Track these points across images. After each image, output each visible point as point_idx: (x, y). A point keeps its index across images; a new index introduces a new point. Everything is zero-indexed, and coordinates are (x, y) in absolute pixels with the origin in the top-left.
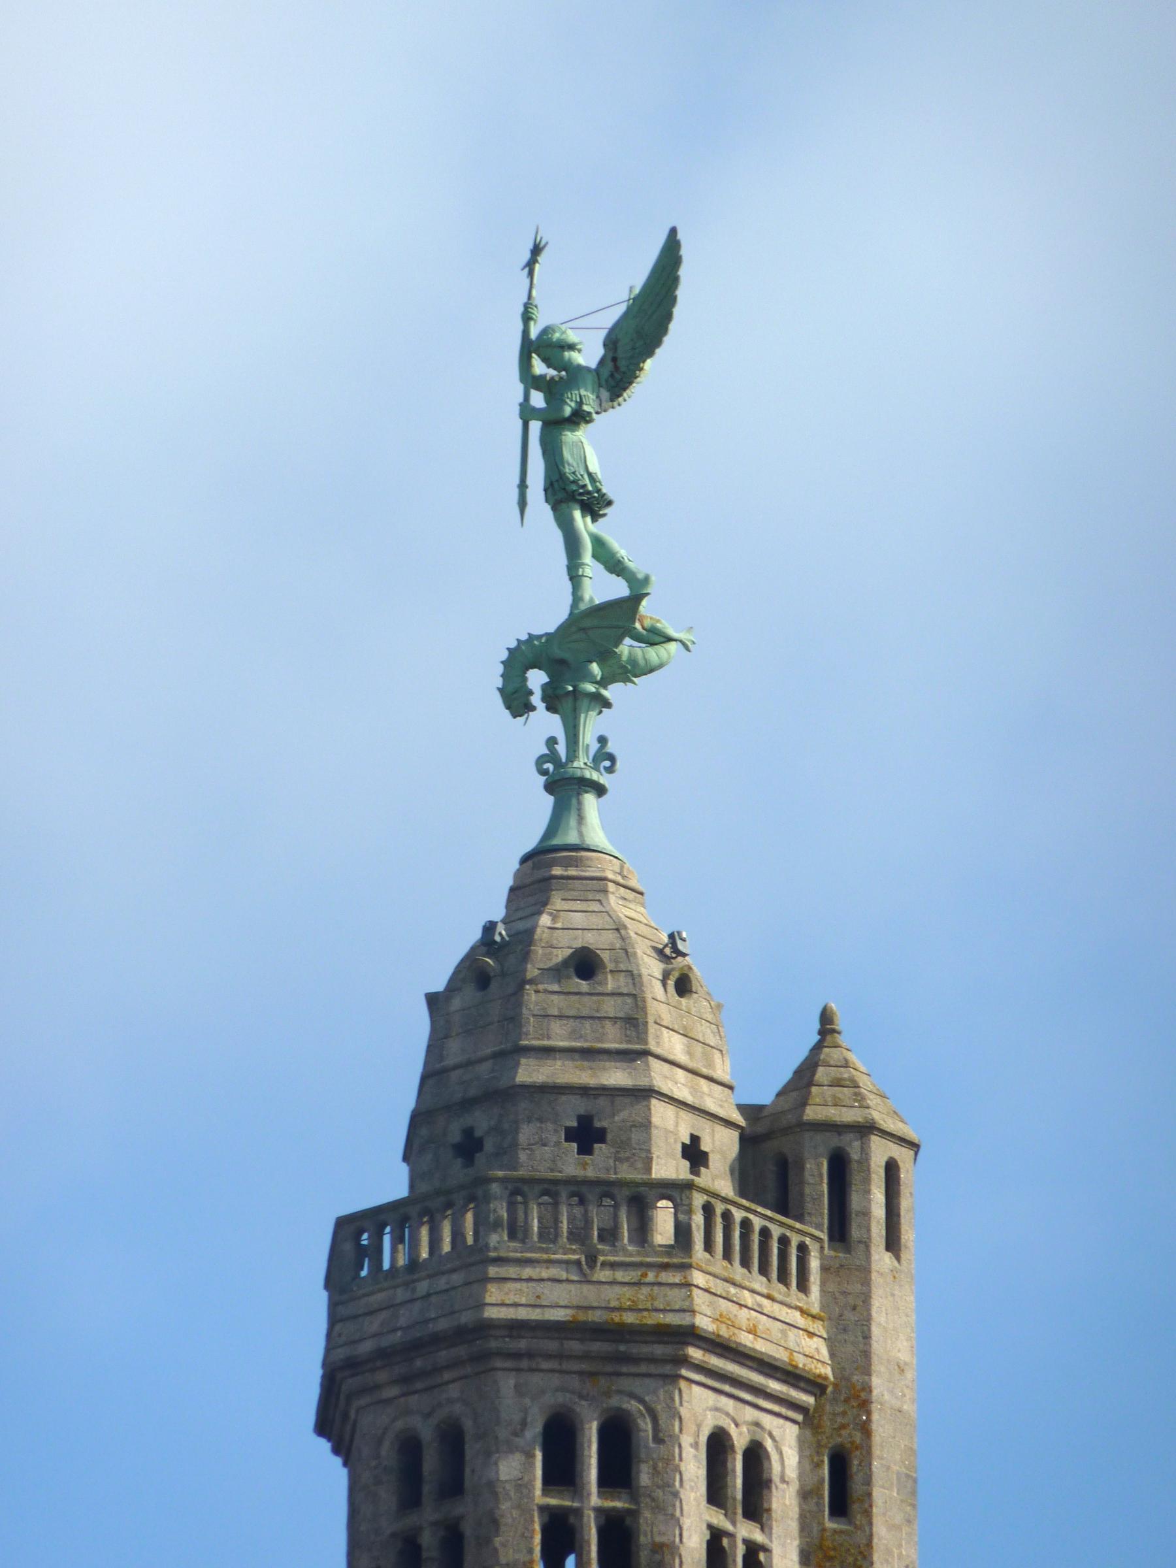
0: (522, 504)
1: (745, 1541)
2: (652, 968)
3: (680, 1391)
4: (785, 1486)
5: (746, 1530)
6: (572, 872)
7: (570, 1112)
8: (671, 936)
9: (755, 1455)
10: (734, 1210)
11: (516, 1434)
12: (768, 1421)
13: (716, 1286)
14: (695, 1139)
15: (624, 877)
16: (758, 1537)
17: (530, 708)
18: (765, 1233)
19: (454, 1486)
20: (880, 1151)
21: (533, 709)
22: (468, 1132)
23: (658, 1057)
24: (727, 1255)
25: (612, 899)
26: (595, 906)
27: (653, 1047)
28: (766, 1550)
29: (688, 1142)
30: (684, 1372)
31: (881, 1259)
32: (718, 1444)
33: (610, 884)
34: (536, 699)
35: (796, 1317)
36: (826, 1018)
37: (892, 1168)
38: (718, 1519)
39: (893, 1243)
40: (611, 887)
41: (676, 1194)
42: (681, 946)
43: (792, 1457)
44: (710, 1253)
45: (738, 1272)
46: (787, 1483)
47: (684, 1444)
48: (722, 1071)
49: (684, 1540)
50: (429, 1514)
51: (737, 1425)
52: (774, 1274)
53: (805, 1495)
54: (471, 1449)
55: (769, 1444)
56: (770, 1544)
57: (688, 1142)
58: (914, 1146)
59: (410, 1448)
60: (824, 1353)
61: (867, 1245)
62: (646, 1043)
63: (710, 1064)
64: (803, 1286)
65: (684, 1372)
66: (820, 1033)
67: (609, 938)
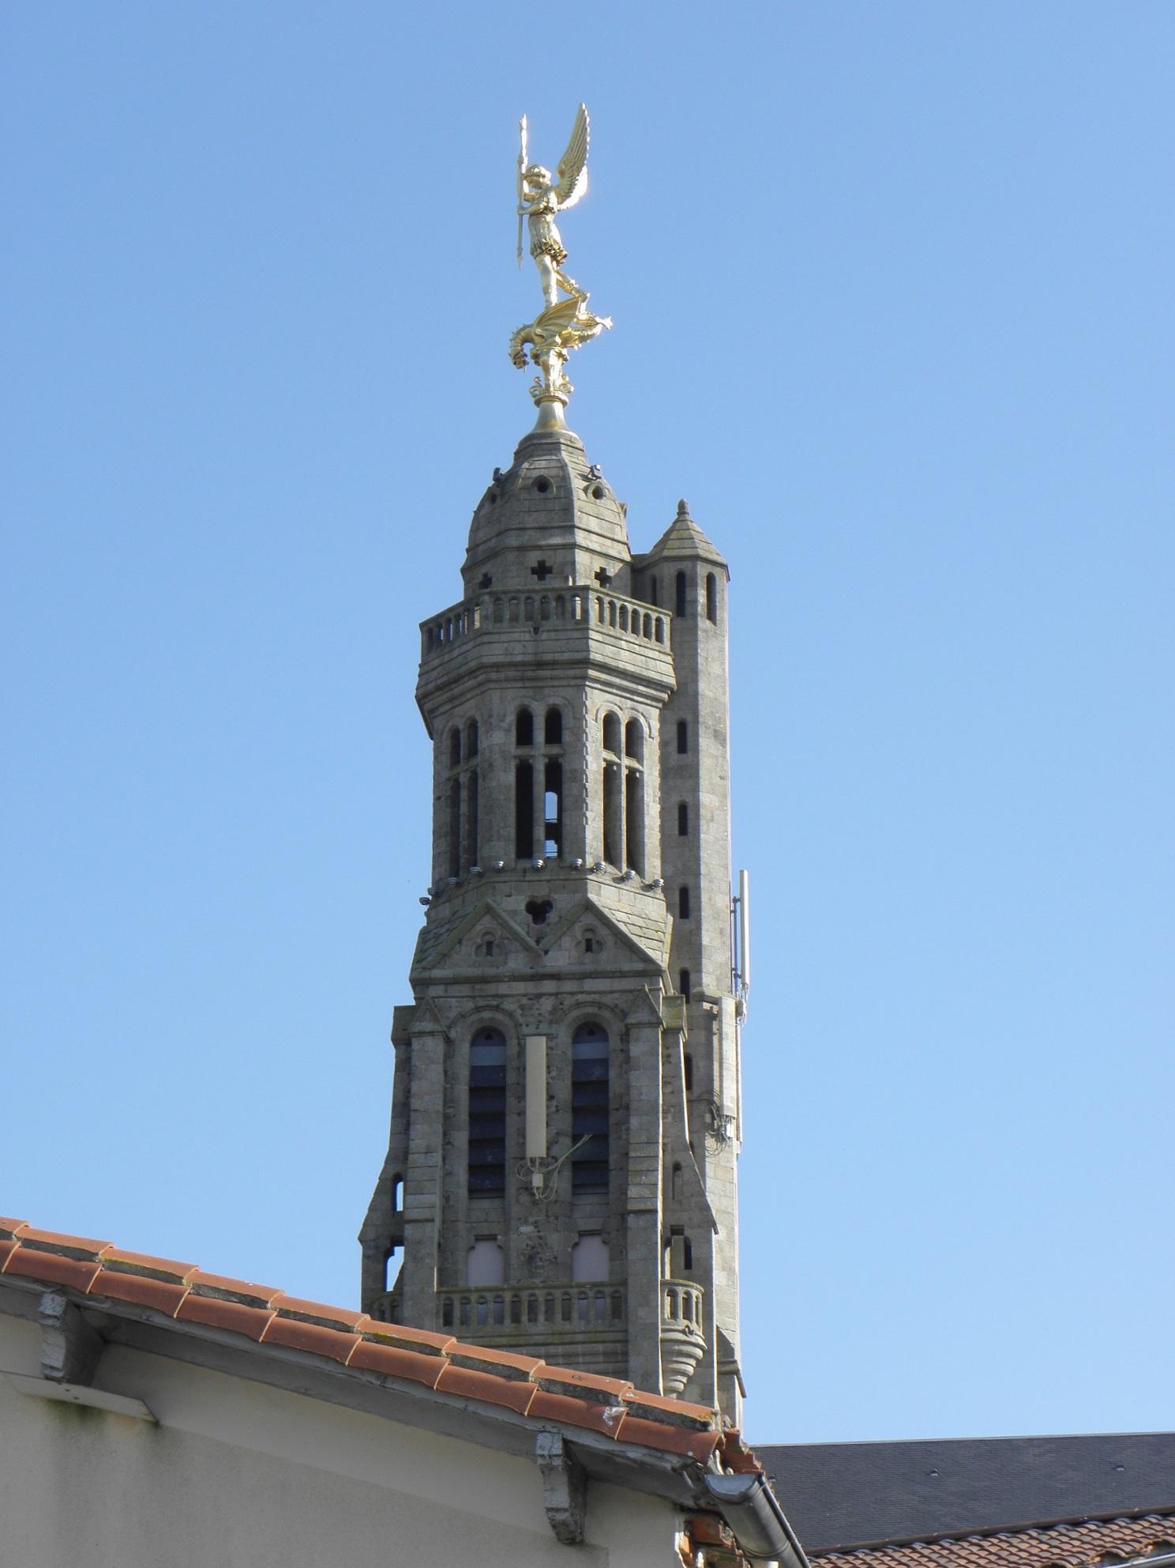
0: (520, 254)
1: (627, 767)
2: (578, 484)
3: (586, 693)
4: (651, 740)
5: (626, 761)
6: (549, 441)
7: (533, 559)
8: (591, 468)
9: (633, 726)
10: (615, 601)
11: (501, 721)
12: (641, 707)
13: (644, 651)
14: (603, 570)
15: (571, 442)
16: (636, 765)
17: (525, 363)
18: (647, 616)
19: (473, 751)
20: (702, 570)
21: (528, 363)
22: (485, 575)
23: (579, 528)
24: (612, 624)
25: (564, 454)
26: (554, 457)
27: (577, 524)
28: (641, 773)
29: (598, 571)
30: (587, 683)
31: (703, 623)
32: (610, 721)
33: (562, 446)
34: (529, 359)
35: (656, 655)
36: (682, 507)
37: (711, 580)
38: (612, 757)
39: (711, 615)
40: (563, 447)
41: (581, 593)
42: (596, 472)
43: (656, 725)
44: (602, 623)
45: (618, 632)
46: (653, 738)
47: (588, 719)
48: (620, 535)
49: (589, 767)
50: (463, 766)
51: (621, 709)
52: (654, 637)
53: (663, 745)
54: (481, 730)
55: (642, 720)
56: (641, 768)
57: (598, 571)
58: (723, 566)
59: (455, 734)
60: (670, 670)
61: (695, 616)
62: (573, 521)
63: (612, 531)
64: (659, 639)
65: (587, 683)
66: (679, 514)
67: (554, 472)
